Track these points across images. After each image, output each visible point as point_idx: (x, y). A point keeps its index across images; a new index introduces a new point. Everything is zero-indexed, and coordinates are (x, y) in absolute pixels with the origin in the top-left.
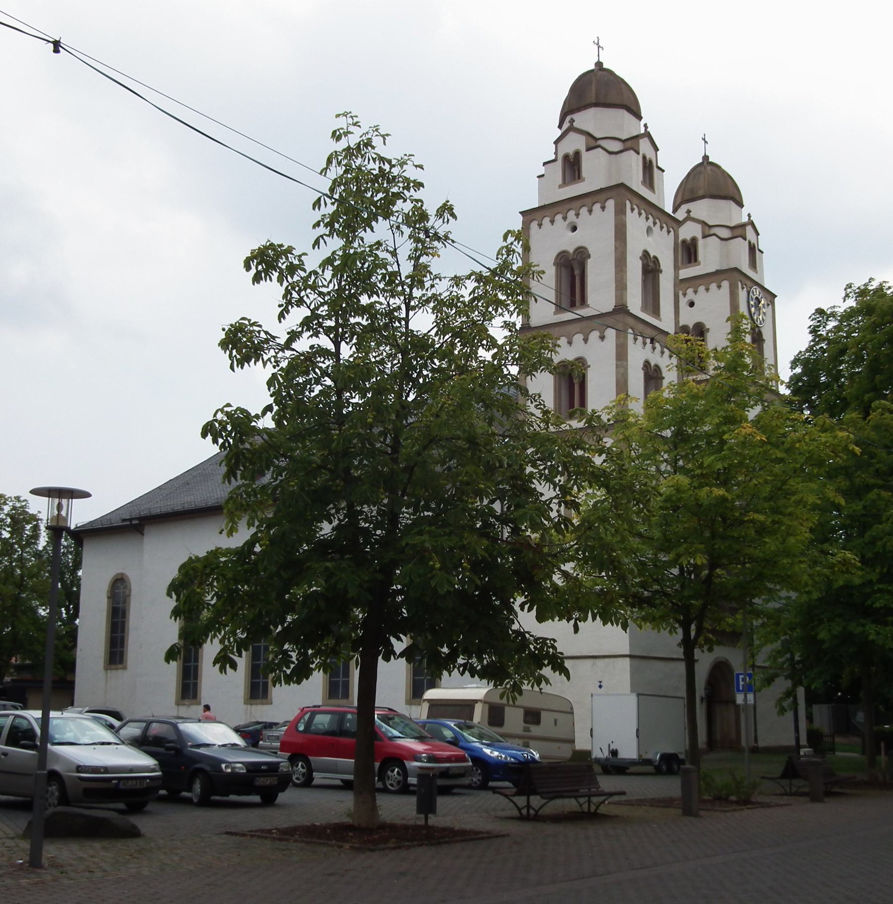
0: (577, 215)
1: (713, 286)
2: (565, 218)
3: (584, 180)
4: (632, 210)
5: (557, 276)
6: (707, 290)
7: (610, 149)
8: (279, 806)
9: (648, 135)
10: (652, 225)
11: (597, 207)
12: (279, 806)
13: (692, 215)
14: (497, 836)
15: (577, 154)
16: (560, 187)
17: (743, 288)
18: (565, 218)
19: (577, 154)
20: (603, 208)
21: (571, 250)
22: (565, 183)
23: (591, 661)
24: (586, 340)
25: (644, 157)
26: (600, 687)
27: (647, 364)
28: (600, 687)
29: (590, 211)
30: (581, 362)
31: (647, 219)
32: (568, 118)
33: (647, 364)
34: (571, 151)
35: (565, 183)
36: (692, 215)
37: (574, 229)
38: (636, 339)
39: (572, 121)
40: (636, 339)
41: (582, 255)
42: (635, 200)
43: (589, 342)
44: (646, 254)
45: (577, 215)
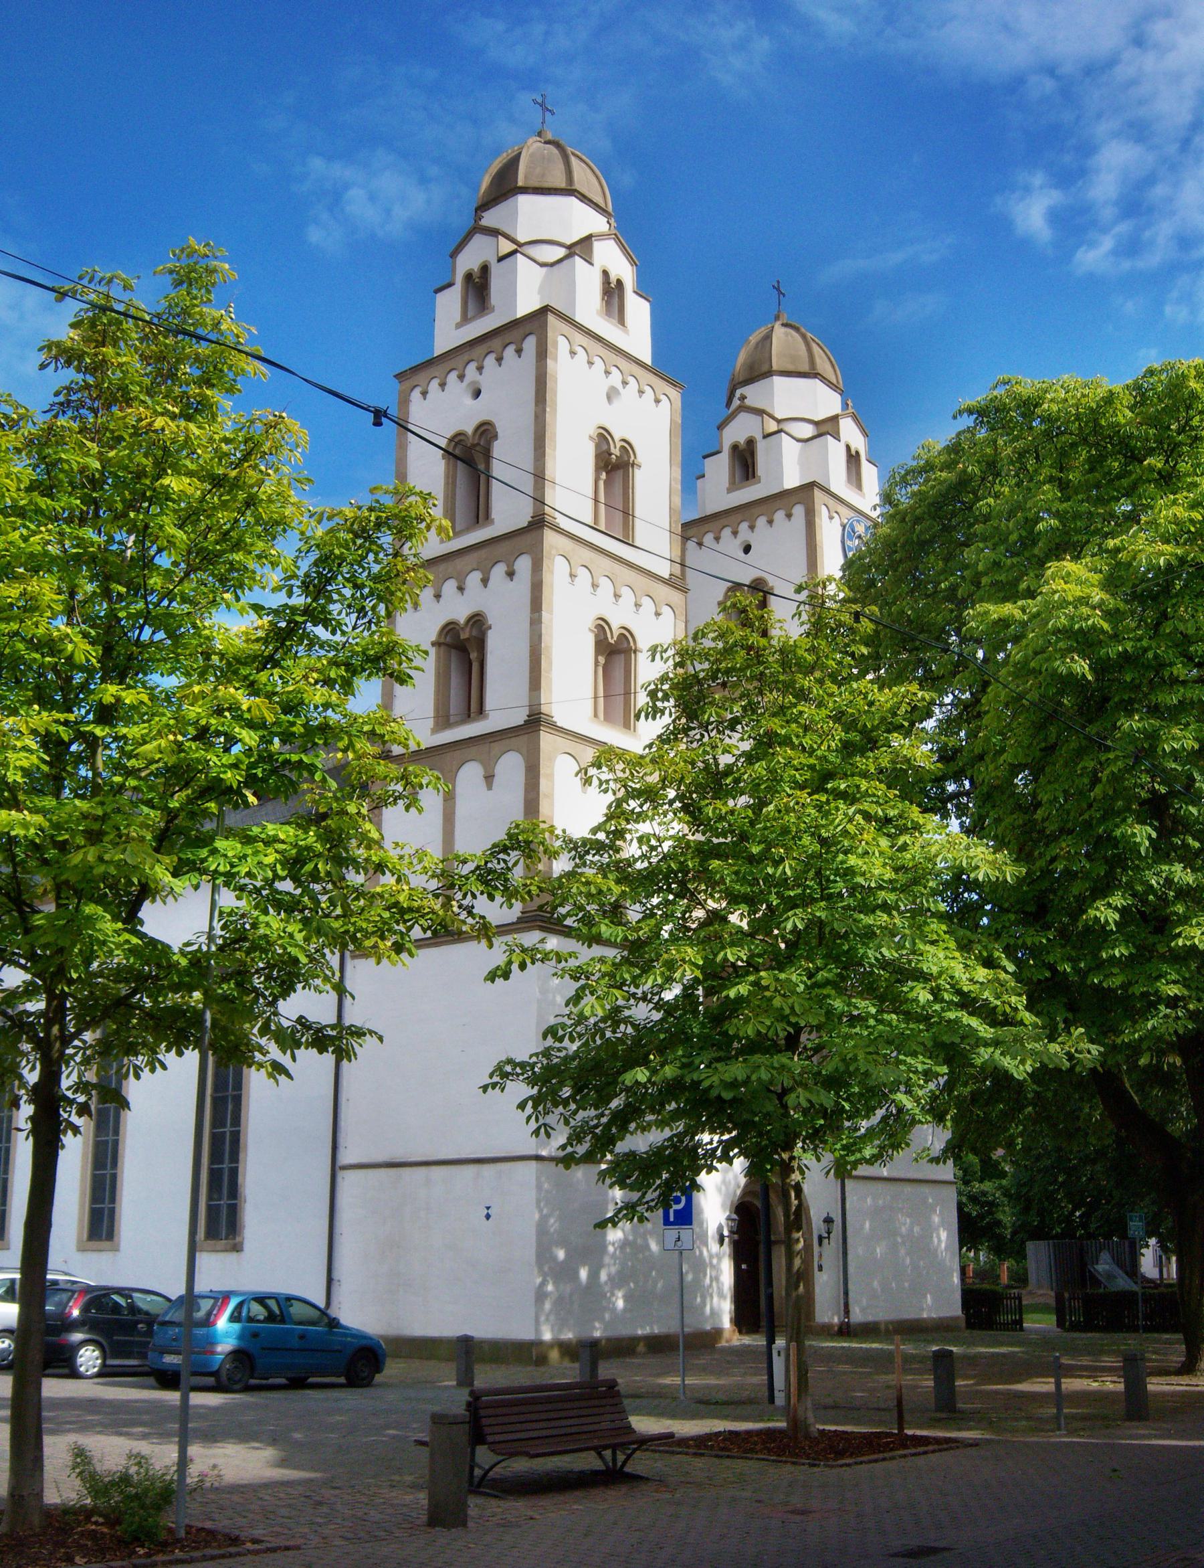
0: (480, 369)
1: (779, 516)
3: (493, 310)
5: (447, 476)
6: (770, 522)
7: (541, 259)
8: (380, 1385)
10: (619, 386)
11: (779, 516)
12: (380, 1385)
13: (747, 402)
14: (835, 1407)
15: (751, 442)
16: (458, 326)
17: (831, 518)
18: (461, 377)
19: (751, 442)
20: (519, 351)
21: (469, 430)
22: (733, 487)
23: (471, 1169)
24: (485, 581)
26: (488, 1217)
27: (602, 627)
28: (488, 1217)
29: (499, 360)
30: (478, 621)
33: (602, 627)
34: (742, 440)
35: (733, 487)
36: (747, 402)
37: (477, 393)
39: (743, 398)
41: (486, 431)
42: (579, 338)
43: (490, 584)
44: (603, 437)
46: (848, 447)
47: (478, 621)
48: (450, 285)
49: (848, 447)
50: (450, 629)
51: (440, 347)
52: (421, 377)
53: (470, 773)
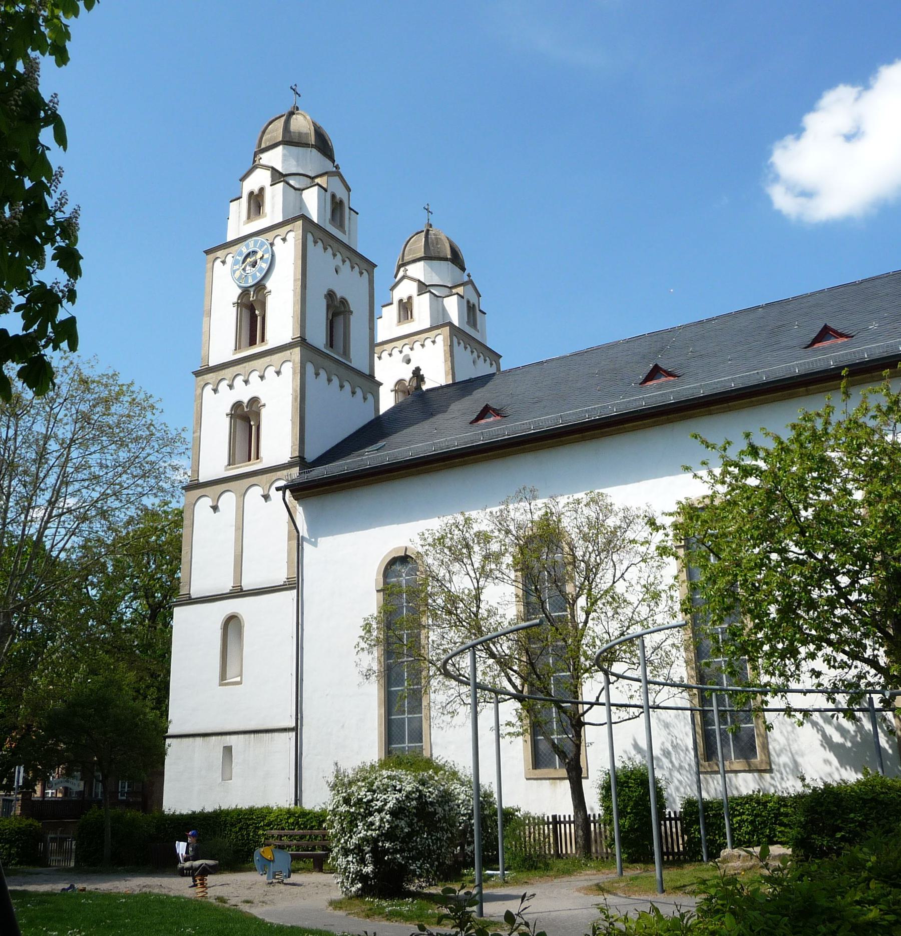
2: (401, 352)
4: (459, 343)
9: (471, 282)
25: (333, 196)
31: (472, 352)
32: (402, 269)
36: (408, 273)
38: (317, 374)
40: (317, 374)
44: (330, 295)
45: (412, 349)
46: (468, 302)
47: (254, 401)
48: (392, 304)
49: (468, 302)
50: (238, 405)
51: (230, 238)
52: (219, 254)
53: (255, 493)
